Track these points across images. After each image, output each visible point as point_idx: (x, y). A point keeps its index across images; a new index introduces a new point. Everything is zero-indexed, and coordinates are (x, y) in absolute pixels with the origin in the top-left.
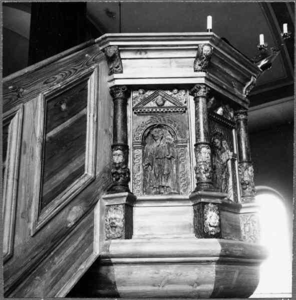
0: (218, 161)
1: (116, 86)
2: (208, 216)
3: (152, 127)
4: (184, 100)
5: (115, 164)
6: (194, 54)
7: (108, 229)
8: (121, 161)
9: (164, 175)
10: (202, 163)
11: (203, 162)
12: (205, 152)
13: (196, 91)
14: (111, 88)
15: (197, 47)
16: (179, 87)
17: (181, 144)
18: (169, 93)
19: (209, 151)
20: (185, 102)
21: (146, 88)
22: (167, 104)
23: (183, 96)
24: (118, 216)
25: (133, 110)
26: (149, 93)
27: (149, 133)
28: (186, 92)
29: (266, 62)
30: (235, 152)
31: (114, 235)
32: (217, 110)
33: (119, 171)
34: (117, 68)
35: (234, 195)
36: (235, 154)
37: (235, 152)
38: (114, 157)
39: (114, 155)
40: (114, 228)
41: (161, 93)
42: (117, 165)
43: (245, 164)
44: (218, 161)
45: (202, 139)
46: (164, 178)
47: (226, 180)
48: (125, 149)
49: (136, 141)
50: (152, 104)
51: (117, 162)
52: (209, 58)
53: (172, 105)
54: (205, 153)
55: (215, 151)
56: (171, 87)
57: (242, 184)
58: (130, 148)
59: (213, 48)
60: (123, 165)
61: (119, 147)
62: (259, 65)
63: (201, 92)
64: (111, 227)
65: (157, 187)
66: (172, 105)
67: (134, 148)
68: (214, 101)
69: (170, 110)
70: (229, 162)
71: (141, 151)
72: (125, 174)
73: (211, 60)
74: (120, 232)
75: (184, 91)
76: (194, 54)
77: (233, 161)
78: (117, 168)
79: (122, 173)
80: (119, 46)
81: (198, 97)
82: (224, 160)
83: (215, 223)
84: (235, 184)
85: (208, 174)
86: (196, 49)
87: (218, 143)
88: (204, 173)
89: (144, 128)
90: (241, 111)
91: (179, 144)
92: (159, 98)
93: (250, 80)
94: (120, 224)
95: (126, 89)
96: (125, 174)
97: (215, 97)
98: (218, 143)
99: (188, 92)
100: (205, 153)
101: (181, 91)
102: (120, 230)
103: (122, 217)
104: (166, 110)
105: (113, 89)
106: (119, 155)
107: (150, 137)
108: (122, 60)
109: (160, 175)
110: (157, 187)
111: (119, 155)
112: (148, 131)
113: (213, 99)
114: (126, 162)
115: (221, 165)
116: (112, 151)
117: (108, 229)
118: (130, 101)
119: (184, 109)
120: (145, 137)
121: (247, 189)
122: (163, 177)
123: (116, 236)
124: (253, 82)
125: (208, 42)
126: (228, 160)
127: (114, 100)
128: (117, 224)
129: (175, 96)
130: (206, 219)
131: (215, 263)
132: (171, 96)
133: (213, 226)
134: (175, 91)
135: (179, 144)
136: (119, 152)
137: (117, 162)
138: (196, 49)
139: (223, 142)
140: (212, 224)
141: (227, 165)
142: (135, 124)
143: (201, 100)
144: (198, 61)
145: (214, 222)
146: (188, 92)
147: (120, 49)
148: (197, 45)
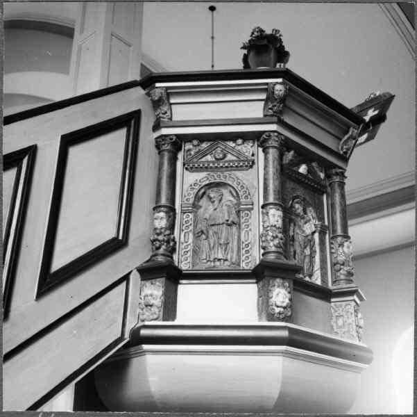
0: (298, 231)
1: (162, 136)
2: (274, 294)
3: (210, 186)
4: (251, 153)
5: (156, 229)
6: (264, 96)
7: (142, 309)
8: (164, 226)
9: (220, 244)
10: (269, 228)
11: (272, 226)
12: (275, 216)
13: (265, 141)
14: (156, 138)
15: (266, 87)
16: (245, 137)
17: (245, 207)
18: (232, 144)
19: (280, 213)
20: (253, 155)
21: (201, 138)
22: (229, 157)
23: (248, 149)
24: (155, 292)
25: (184, 165)
26: (205, 145)
27: (204, 193)
28: (254, 143)
29: (376, 112)
30: (326, 223)
31: (148, 316)
32: (299, 168)
33: (161, 238)
34: (163, 114)
35: (322, 276)
36: (325, 226)
37: (326, 223)
38: (155, 221)
39: (156, 219)
40: (149, 307)
41: (221, 145)
42: (158, 231)
43: (339, 239)
44: (298, 231)
45: (271, 199)
46: (222, 248)
47: (312, 257)
48: (171, 210)
49: (186, 202)
50: (209, 158)
51: (159, 227)
52: (283, 100)
53: (234, 158)
54: (274, 215)
55: (289, 218)
56: (233, 137)
57: (334, 265)
58: (177, 211)
59: (288, 87)
60: (165, 231)
61: (162, 209)
62: (366, 115)
63: (272, 142)
64: (146, 306)
65: (212, 259)
66: (234, 158)
67: (183, 212)
68: (319, 176)
69: (231, 164)
70: (316, 236)
71: (191, 216)
72: (168, 242)
73: (287, 103)
74: (157, 313)
75: (251, 141)
76: (264, 96)
77: (322, 233)
78: (158, 234)
79: (163, 240)
80: (168, 88)
81: (268, 148)
82: (308, 232)
83: (283, 302)
84: (323, 261)
85: (276, 241)
86: (266, 90)
87: (298, 209)
88: (272, 241)
89: (197, 187)
90: (334, 171)
91: (242, 207)
92: (219, 150)
93: (347, 132)
94: (158, 302)
95: (174, 140)
96: (168, 242)
97: (295, 152)
98: (298, 209)
99: (256, 143)
100: (274, 215)
101: (247, 142)
102: (157, 310)
103: (160, 293)
104: (226, 164)
105: (158, 140)
106: (162, 218)
107: (205, 198)
108: (173, 106)
109: (217, 246)
110: (212, 259)
111: (162, 218)
112: (203, 191)
113: (292, 153)
114: (171, 227)
115: (304, 238)
116: (154, 214)
117: (142, 309)
118: (180, 156)
119: (251, 163)
120: (198, 198)
121: (341, 271)
122: (220, 248)
123: (151, 317)
124: (351, 135)
125: (280, 80)
126: (315, 232)
127: (159, 153)
128: (152, 302)
129: (239, 148)
130: (271, 298)
131: (165, 209)
132: (234, 148)
133: (281, 307)
134: (240, 141)
135: (242, 207)
136: (162, 214)
137: (159, 227)
138: (266, 90)
139: (307, 209)
140: (279, 304)
141: (313, 238)
142: (188, 181)
143: (271, 151)
144: (269, 103)
145: (282, 300)
146: (256, 143)
147: (169, 91)
148: (267, 84)
